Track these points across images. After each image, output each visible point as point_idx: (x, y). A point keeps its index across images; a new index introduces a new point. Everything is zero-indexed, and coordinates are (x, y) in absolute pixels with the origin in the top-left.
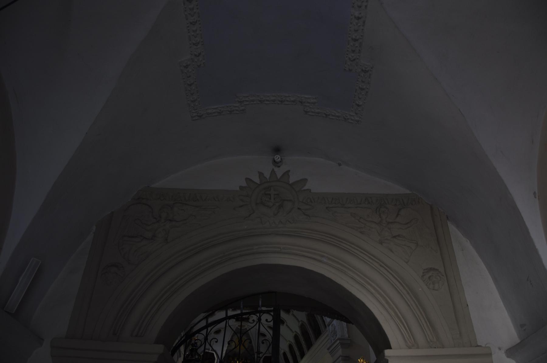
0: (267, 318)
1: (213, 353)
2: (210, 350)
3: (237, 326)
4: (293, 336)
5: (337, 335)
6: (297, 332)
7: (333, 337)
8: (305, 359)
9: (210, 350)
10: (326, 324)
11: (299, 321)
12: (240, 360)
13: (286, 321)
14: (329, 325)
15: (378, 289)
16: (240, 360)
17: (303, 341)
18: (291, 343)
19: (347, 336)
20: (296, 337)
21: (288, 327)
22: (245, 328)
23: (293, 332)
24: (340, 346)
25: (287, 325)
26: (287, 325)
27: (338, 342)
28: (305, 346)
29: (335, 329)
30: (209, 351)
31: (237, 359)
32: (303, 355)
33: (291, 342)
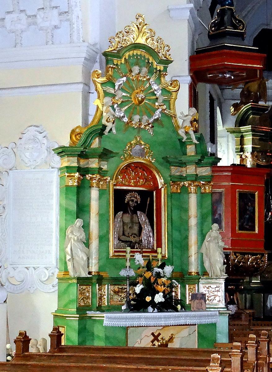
17: (22, 362)
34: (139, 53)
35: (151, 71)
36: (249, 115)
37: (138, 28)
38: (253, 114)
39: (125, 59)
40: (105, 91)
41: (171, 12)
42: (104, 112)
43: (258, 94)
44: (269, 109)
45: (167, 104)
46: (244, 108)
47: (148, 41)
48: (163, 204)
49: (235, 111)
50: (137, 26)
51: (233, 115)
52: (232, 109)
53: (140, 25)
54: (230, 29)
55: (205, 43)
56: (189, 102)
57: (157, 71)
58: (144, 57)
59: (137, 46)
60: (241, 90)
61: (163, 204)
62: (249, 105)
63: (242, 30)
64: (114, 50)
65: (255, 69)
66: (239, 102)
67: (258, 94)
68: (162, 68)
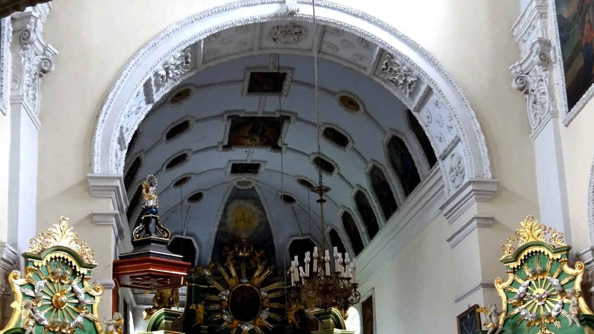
0: (316, 201)
1: (176, 238)
2: (184, 234)
3: (234, 183)
4: (352, 195)
5: (464, 175)
6: (361, 187)
7: (453, 182)
8: (378, 238)
9: (184, 234)
10: (437, 155)
11: (367, 163)
12: (245, 249)
13: (337, 165)
14: (444, 158)
15: (465, 200)
16: (245, 249)
17: (376, 202)
18: (347, 210)
19: (490, 175)
20: (360, 198)
21: (342, 177)
22: (250, 187)
23: (353, 188)
24: (474, 197)
25: (339, 174)
26: (339, 174)
27: (470, 188)
28: (378, 211)
29: (460, 162)
30: (183, 237)
31: (239, 249)
32: (373, 230)
33: (348, 209)
34: (61, 256)
35: (75, 273)
36: (162, 319)
37: (62, 231)
38: (166, 319)
39: (47, 261)
40: (24, 294)
41: (94, 217)
42: (23, 314)
43: (171, 299)
44: (181, 314)
45: (90, 308)
46: (157, 313)
47: (72, 244)
48: (307, 269)
49: (147, 316)
50: (60, 228)
51: (145, 319)
52: (145, 314)
53: (63, 227)
54: (154, 237)
55: (129, 249)
56: (13, 315)
57: (80, 274)
58: (67, 259)
59: (59, 249)
60: (154, 295)
61: (307, 269)
62: (162, 310)
63: (167, 238)
64: (35, 251)
65: (179, 277)
66: (151, 307)
67: (171, 299)
68: (86, 273)
